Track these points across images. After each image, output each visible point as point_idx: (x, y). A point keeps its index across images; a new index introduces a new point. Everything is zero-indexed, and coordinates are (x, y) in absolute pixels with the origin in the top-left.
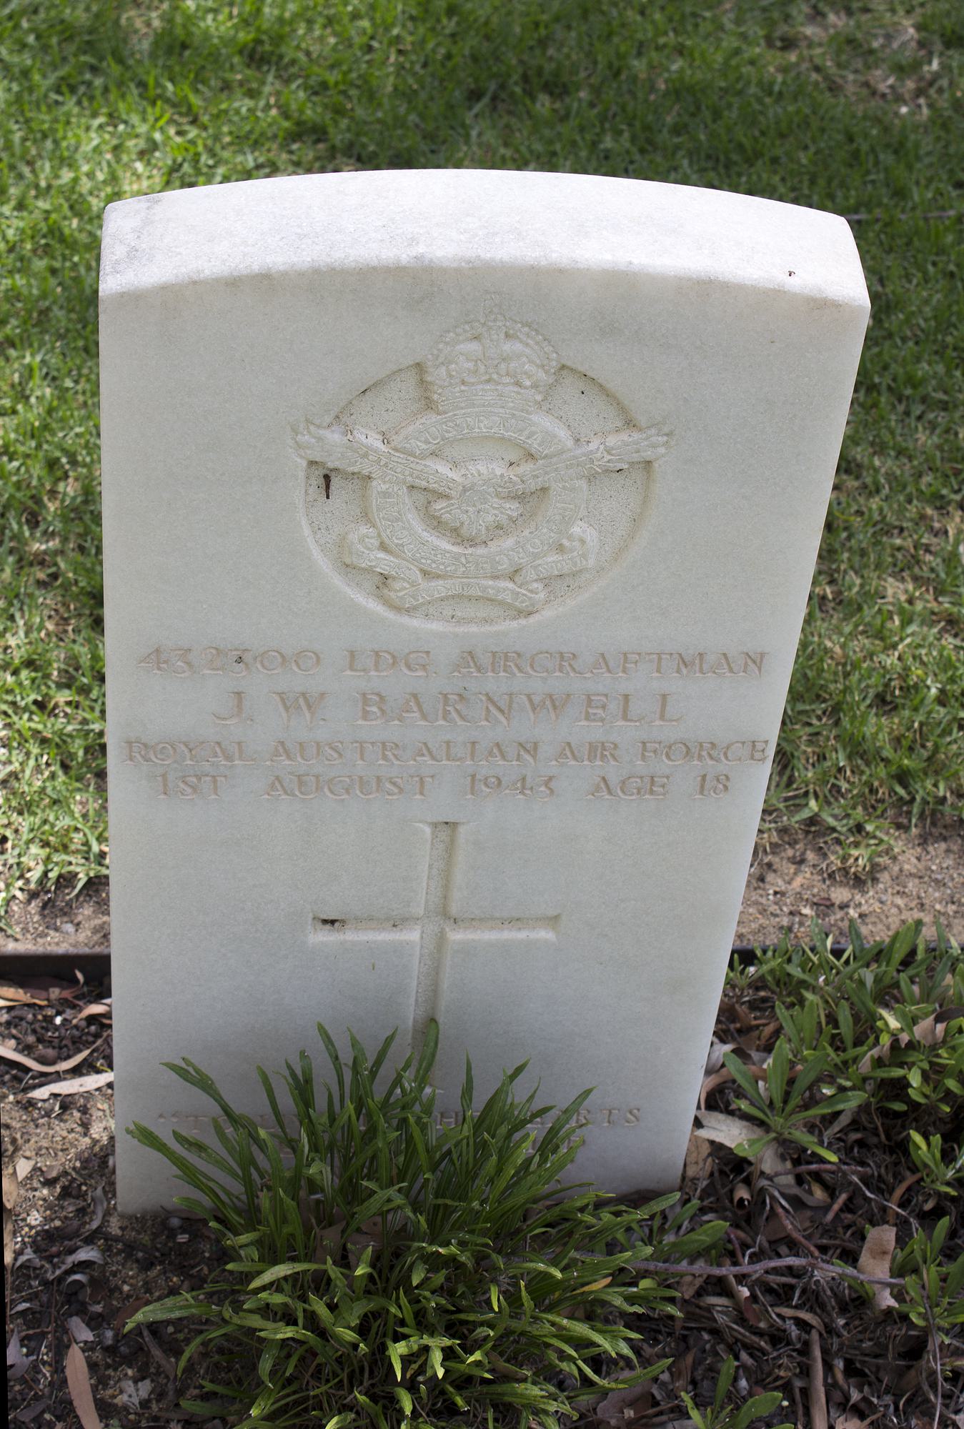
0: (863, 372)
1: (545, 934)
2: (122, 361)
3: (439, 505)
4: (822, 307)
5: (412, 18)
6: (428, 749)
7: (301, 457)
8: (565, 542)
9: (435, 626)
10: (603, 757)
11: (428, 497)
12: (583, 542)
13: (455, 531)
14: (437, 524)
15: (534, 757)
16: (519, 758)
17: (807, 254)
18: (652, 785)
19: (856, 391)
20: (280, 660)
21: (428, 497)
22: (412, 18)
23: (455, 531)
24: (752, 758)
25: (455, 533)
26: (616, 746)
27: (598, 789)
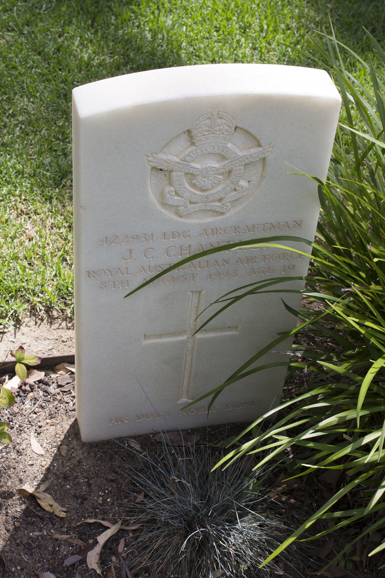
8: (237, 188)
11: (191, 176)
21: (191, 176)
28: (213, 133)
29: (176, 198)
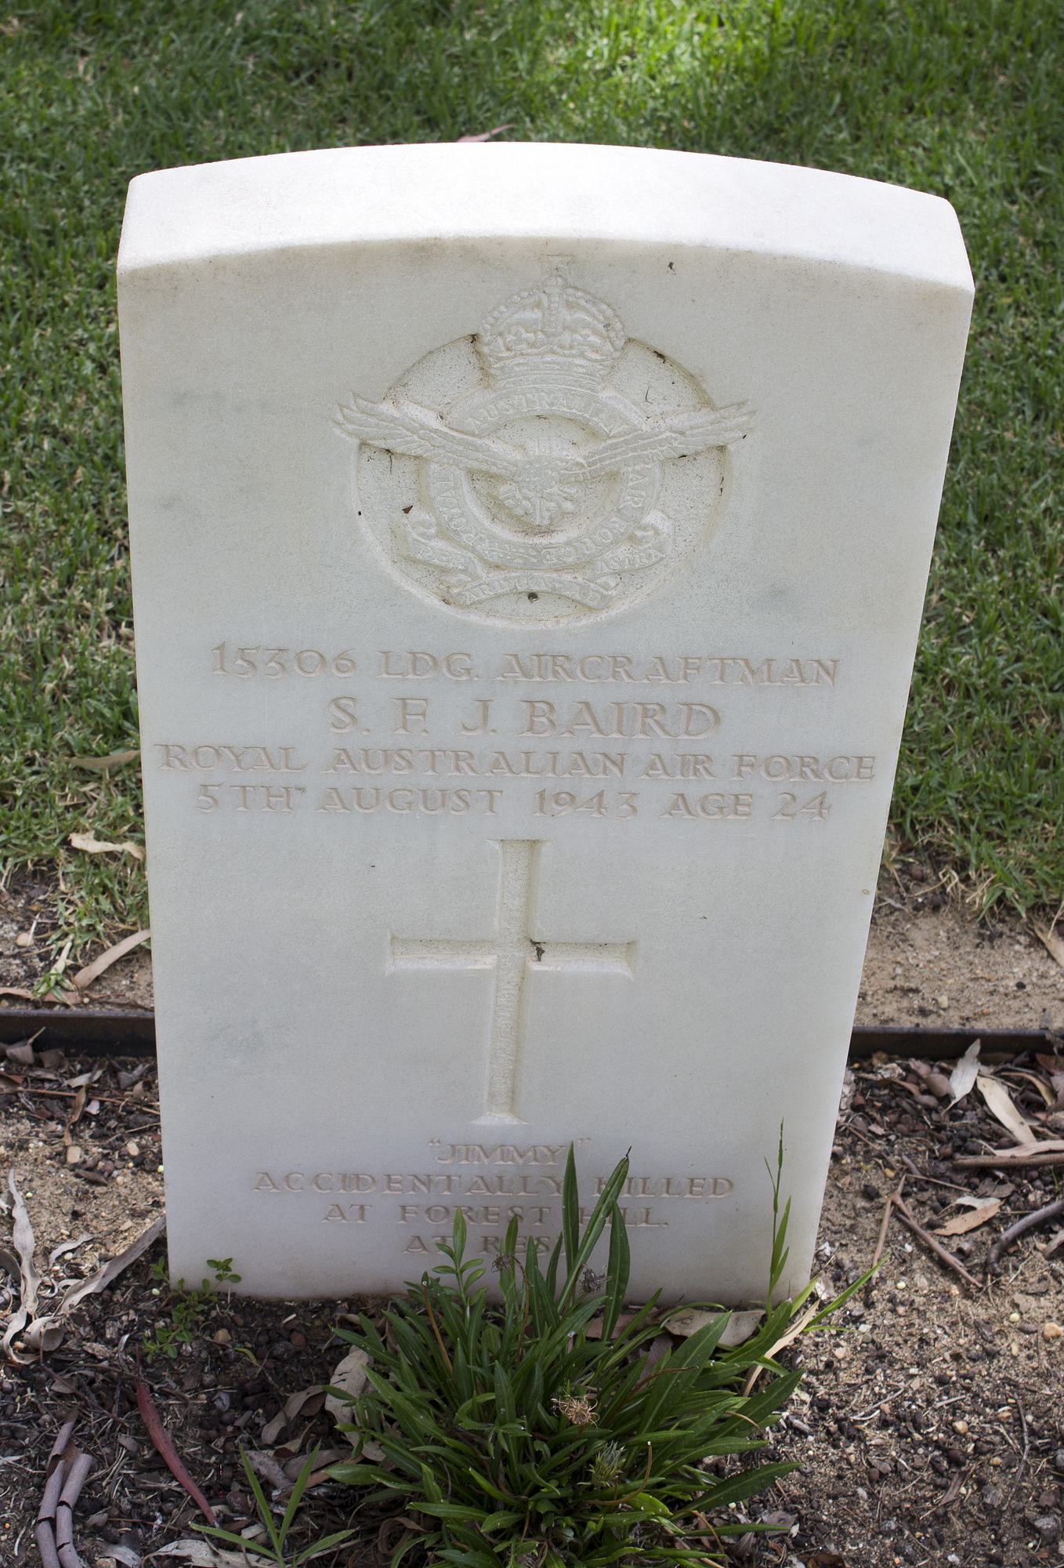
0: (944, 511)
1: (615, 967)
2: (125, 302)
3: (503, 489)
4: (936, 296)
5: (977, 946)
6: (348, 756)
7: (350, 434)
8: (639, 533)
9: (500, 624)
10: (696, 772)
11: (485, 478)
12: (657, 532)
13: (518, 519)
14: (497, 508)
15: (621, 771)
16: (605, 770)
17: (908, 237)
18: (738, 803)
19: (954, 459)
20: (711, 717)
21: (485, 478)
22: (977, 946)
23: (518, 519)
24: (858, 776)
25: (527, 527)
26: (471, 756)
27: (675, 806)
28: (554, 352)
29: (438, 544)
